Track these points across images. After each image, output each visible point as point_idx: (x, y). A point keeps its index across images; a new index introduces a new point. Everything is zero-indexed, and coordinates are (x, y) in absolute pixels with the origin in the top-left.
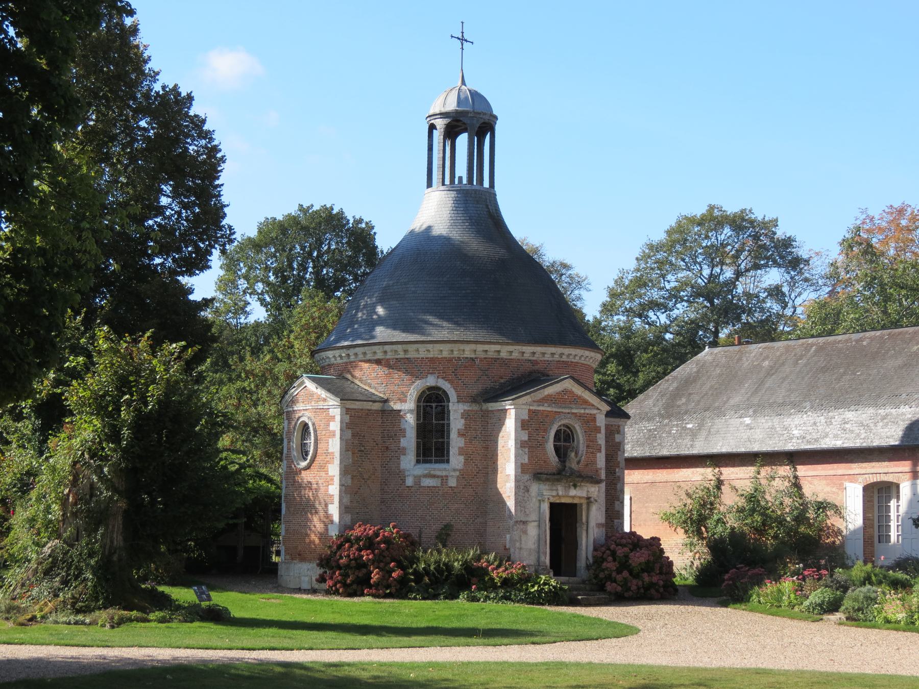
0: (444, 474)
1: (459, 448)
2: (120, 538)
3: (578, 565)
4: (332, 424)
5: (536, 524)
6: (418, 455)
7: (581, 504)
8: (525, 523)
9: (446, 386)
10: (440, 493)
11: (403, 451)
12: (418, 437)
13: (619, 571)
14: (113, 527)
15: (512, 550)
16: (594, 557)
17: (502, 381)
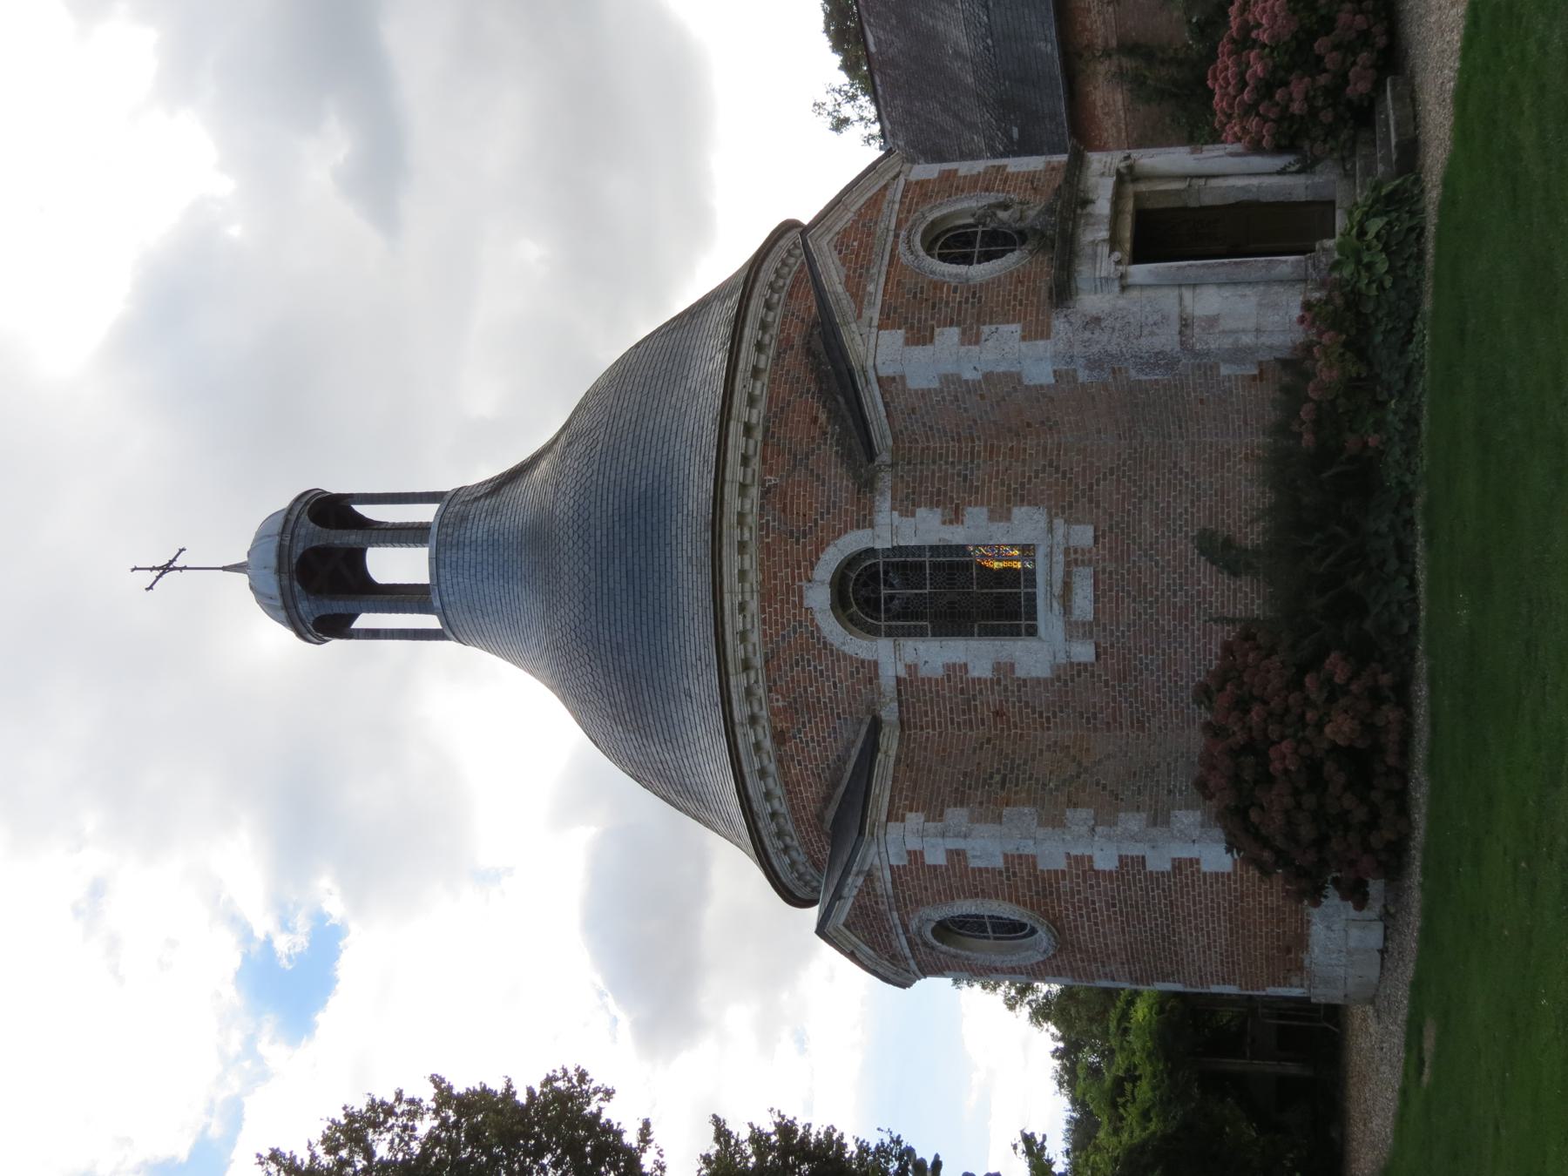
0: (1059, 558)
1: (991, 519)
3: (1301, 195)
4: (930, 859)
6: (1015, 632)
7: (1138, 197)
8: (1185, 323)
10: (1111, 567)
11: (1004, 670)
12: (966, 633)
15: (1266, 356)
17: (823, 417)
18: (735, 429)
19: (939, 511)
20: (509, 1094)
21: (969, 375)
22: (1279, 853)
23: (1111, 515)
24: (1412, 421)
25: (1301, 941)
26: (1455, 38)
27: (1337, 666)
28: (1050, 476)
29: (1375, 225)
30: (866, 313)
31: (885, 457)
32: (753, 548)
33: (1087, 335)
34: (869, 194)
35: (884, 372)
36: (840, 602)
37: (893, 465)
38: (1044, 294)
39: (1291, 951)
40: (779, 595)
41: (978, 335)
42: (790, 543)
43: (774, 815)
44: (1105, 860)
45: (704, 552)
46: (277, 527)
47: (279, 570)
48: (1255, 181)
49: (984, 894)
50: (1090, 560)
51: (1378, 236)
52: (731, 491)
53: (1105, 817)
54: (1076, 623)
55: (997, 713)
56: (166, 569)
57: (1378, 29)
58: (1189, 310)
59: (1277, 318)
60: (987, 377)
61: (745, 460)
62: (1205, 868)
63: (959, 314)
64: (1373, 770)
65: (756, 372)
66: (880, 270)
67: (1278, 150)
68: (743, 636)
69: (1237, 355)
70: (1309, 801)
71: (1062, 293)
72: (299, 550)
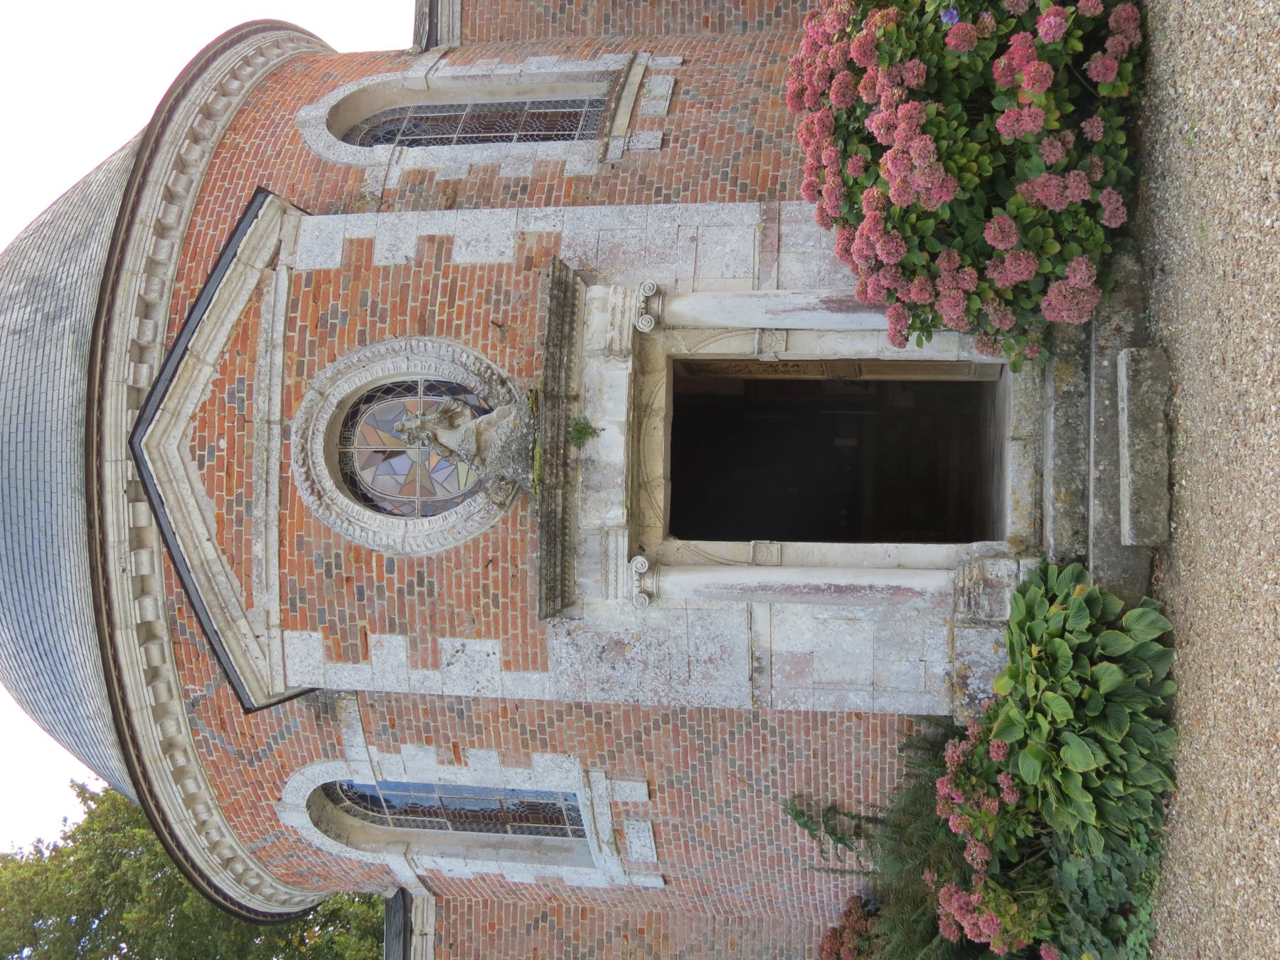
18: (126, 640)
19: (432, 748)
23: (669, 770)
28: (580, 719)
30: (260, 599)
33: (605, 669)
34: (233, 317)
41: (436, 651)
50: (646, 814)
54: (636, 862)
58: (764, 642)
59: (904, 667)
63: (402, 613)
71: (558, 595)
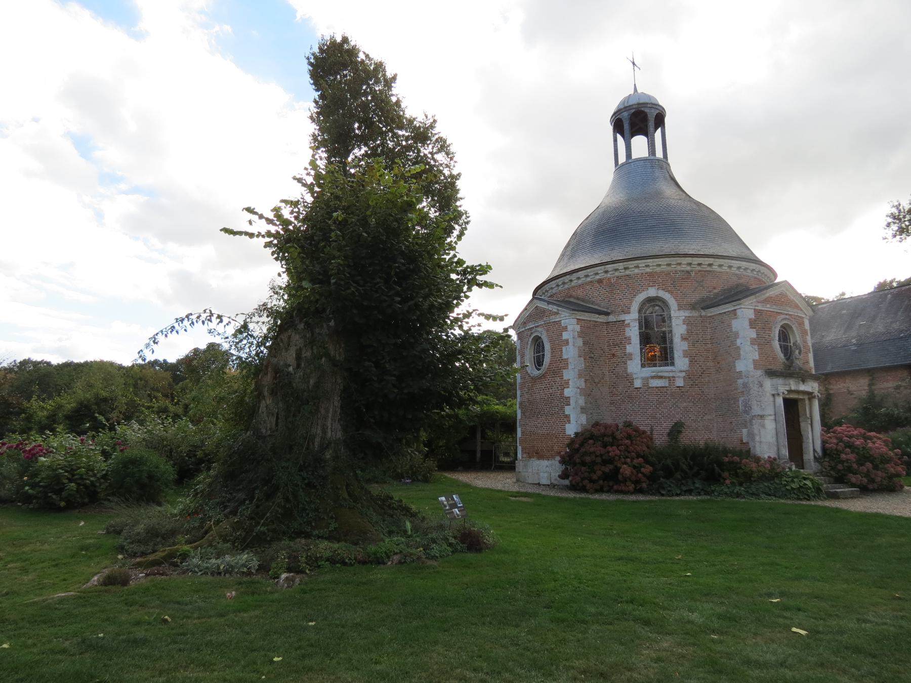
0: (671, 375)
2: (337, 426)
3: (806, 457)
4: (564, 334)
5: (772, 417)
7: (803, 400)
8: (762, 417)
9: (666, 296)
11: (630, 357)
13: (861, 463)
14: (327, 411)
16: (824, 442)
17: (716, 291)
18: (711, 260)
20: (457, 200)
21: (739, 341)
22: (577, 450)
24: (738, 495)
25: (540, 456)
26: (897, 513)
27: (647, 469)
29: (808, 483)
31: (703, 313)
32: (669, 268)
35: (739, 312)
36: (650, 300)
37: (701, 316)
38: (770, 367)
39: (537, 454)
40: (652, 278)
42: (672, 282)
43: (571, 281)
44: (567, 392)
45: (667, 251)
46: (653, 102)
47: (638, 104)
48: (811, 441)
49: (552, 353)
51: (805, 484)
52: (689, 260)
53: (583, 392)
55: (614, 355)
56: (634, 63)
57: (876, 486)
60: (739, 348)
61: (699, 264)
62: (567, 425)
64: (611, 481)
65: (730, 267)
66: (774, 309)
67: (824, 449)
68: (637, 267)
69: (751, 435)
70: (599, 460)
71: (771, 374)
72: (646, 110)
